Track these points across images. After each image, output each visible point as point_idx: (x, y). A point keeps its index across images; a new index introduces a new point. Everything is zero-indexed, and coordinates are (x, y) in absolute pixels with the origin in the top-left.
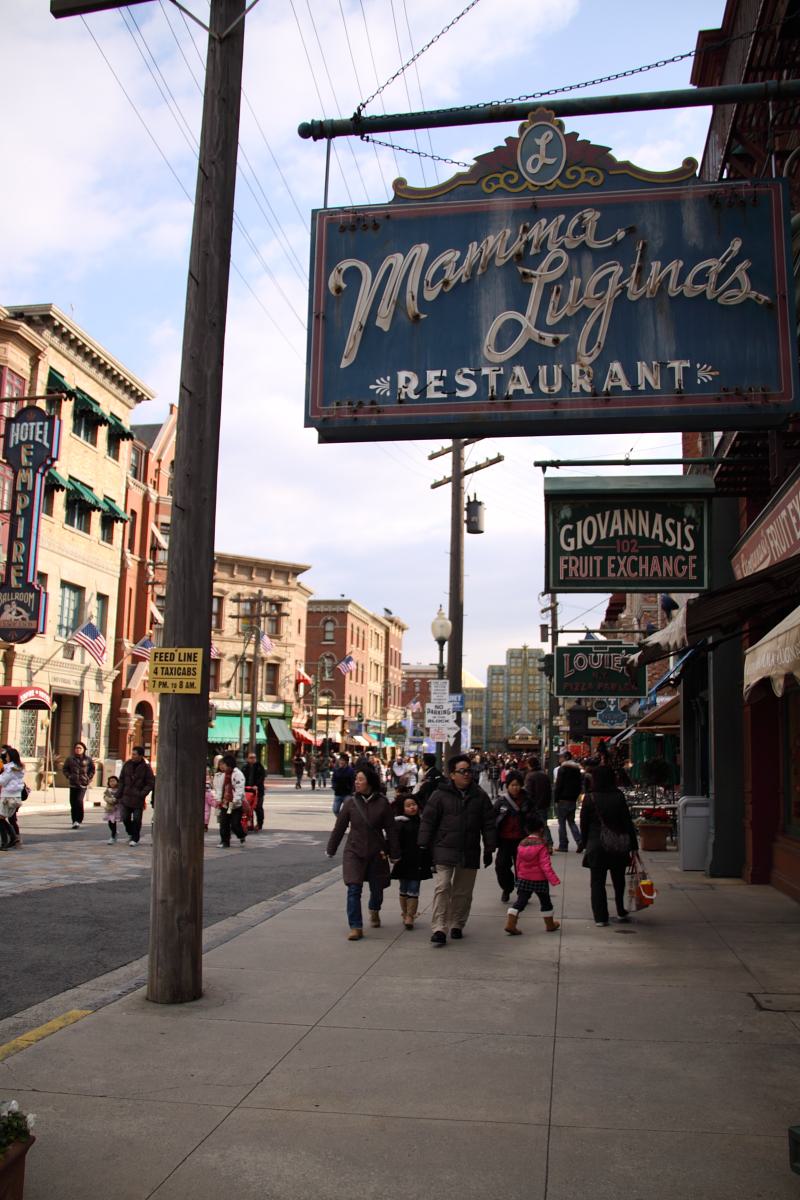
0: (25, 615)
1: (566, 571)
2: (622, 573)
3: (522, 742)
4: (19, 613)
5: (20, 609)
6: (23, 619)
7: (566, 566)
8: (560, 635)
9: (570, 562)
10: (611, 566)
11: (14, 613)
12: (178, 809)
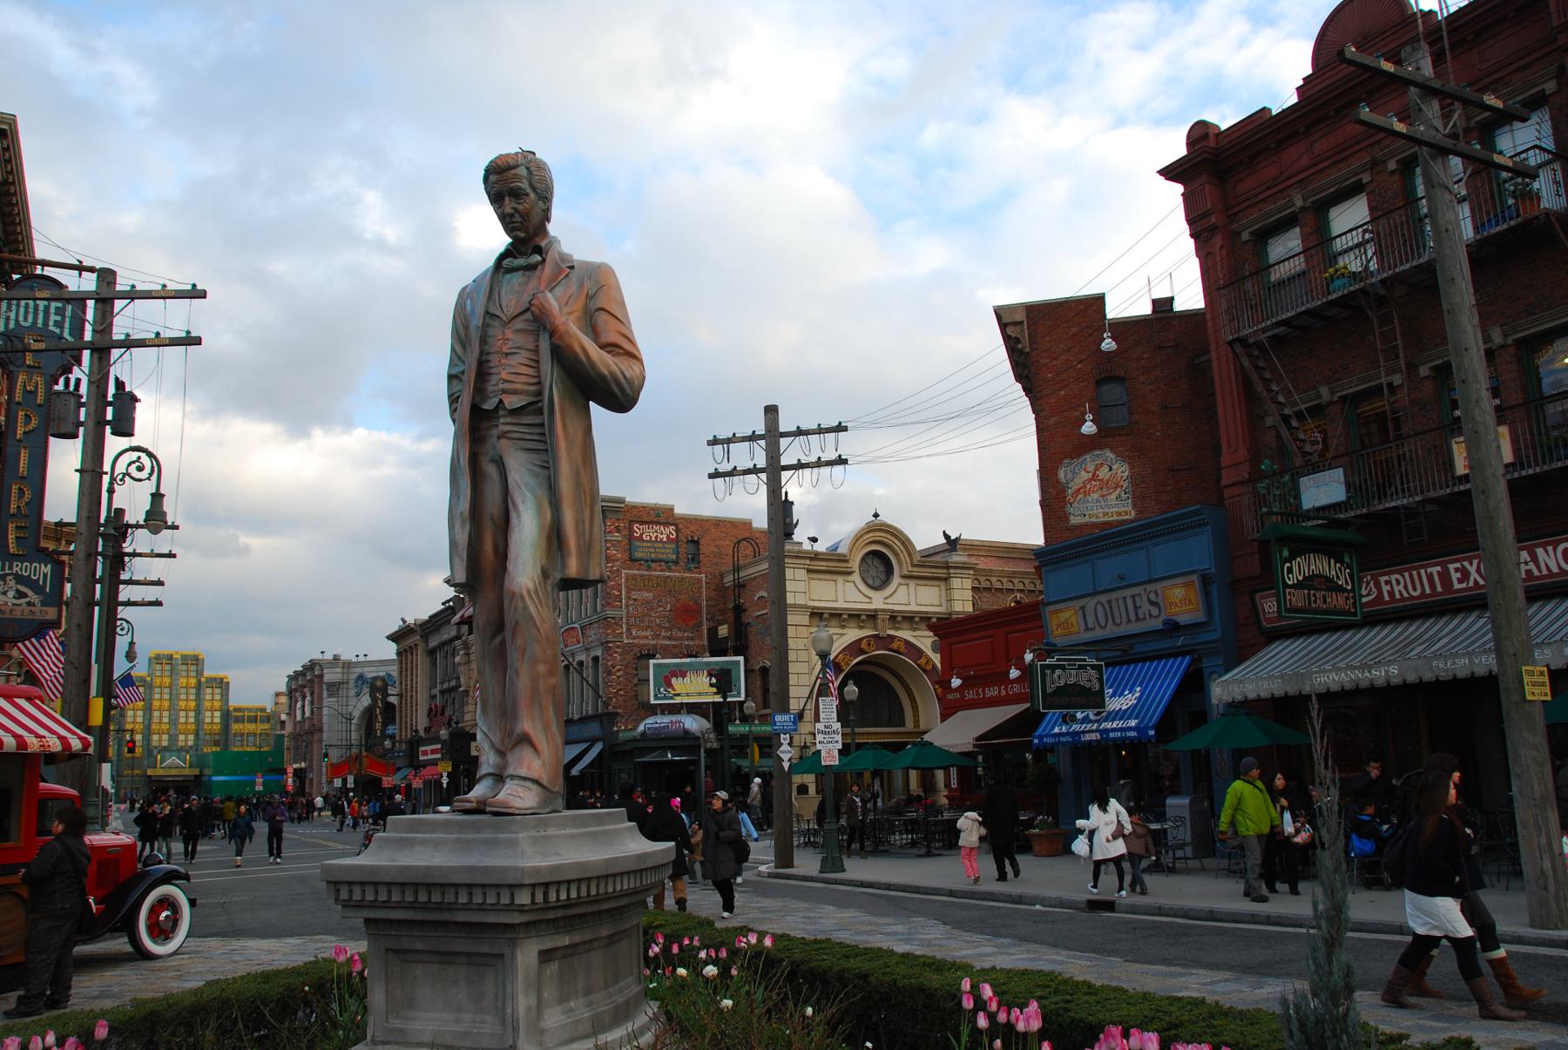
0: (33, 597)
1: (1391, 593)
2: (1475, 580)
3: (31, 617)
4: (21, 595)
5: (22, 588)
6: (29, 604)
7: (1388, 588)
8: (761, 430)
9: (1394, 582)
10: (1455, 576)
11: (11, 594)
12: (419, 946)
